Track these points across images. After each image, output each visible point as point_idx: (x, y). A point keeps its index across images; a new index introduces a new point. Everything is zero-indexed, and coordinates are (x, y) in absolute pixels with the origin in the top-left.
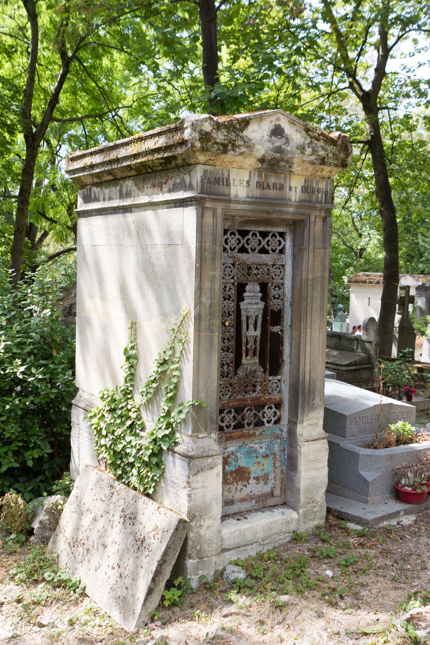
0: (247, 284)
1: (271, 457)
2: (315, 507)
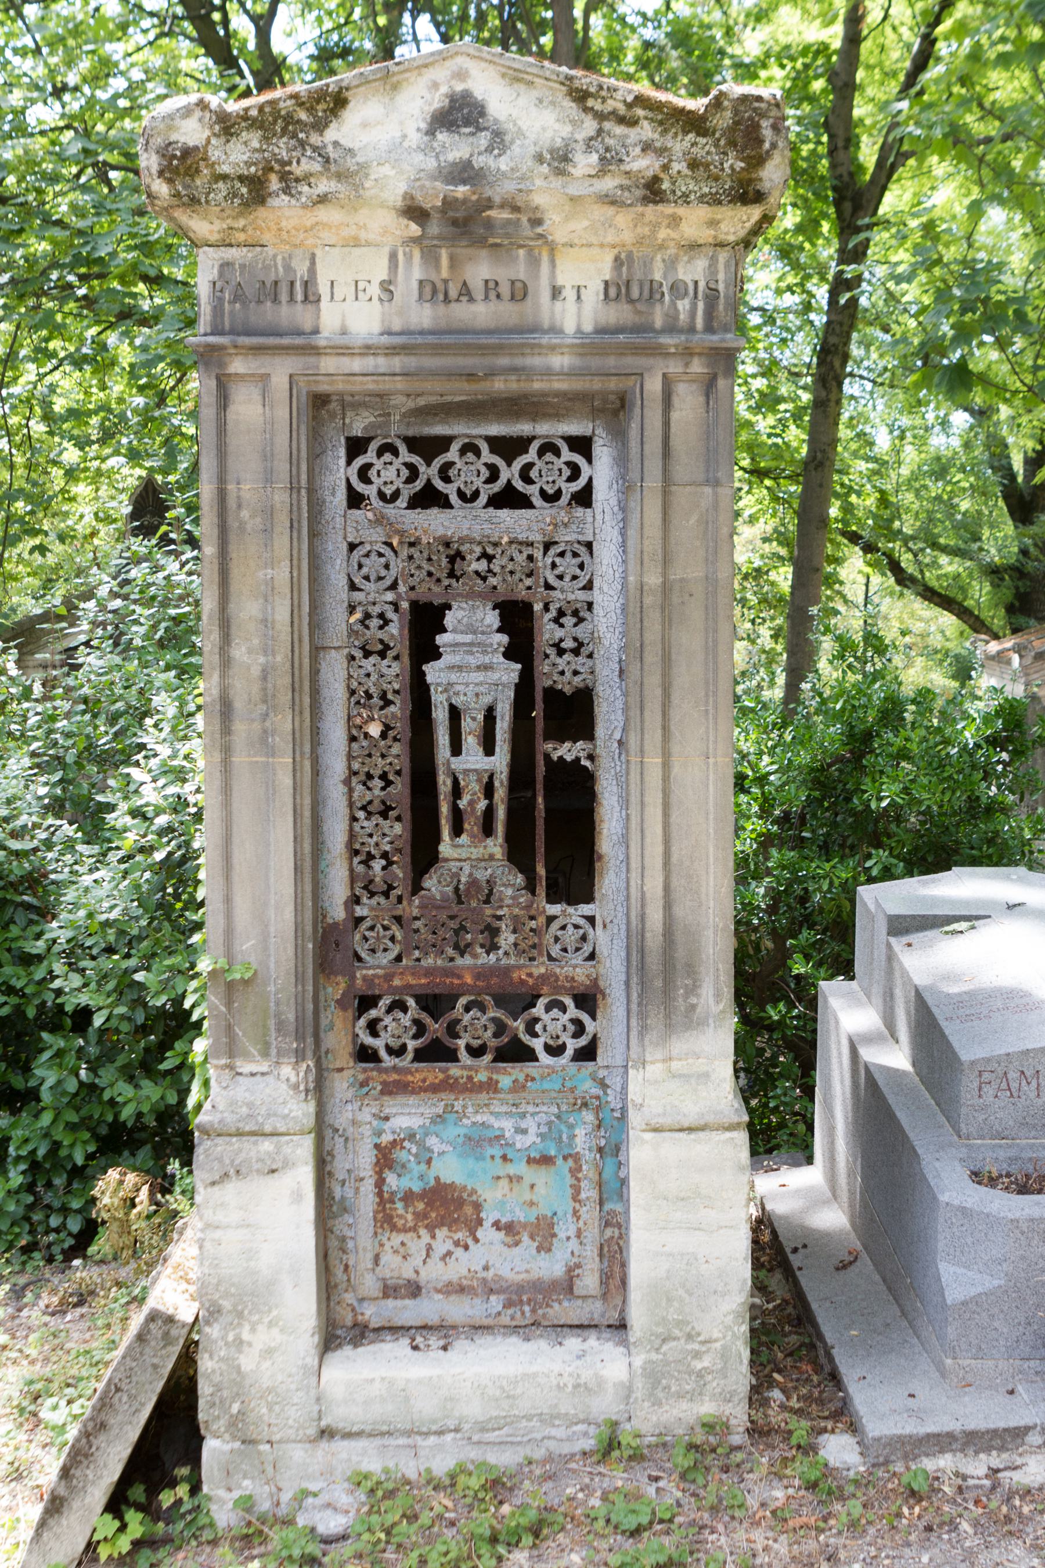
1: (563, 1167)
2: (697, 1355)
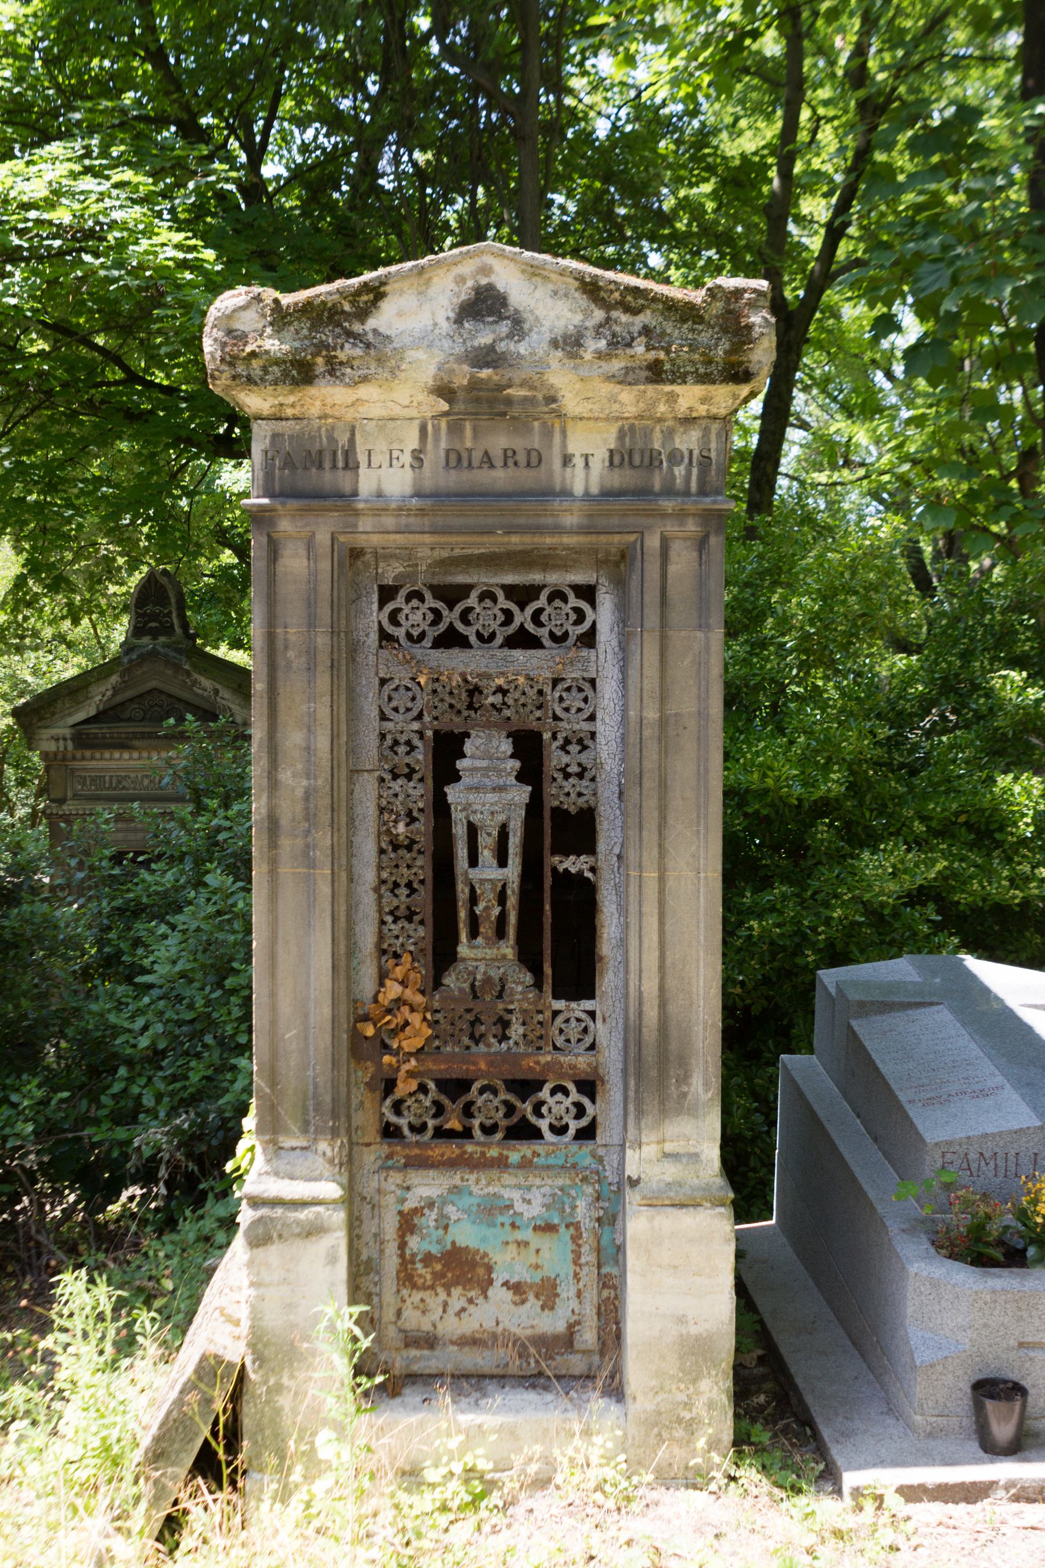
0: (468, 735)
1: (565, 1234)
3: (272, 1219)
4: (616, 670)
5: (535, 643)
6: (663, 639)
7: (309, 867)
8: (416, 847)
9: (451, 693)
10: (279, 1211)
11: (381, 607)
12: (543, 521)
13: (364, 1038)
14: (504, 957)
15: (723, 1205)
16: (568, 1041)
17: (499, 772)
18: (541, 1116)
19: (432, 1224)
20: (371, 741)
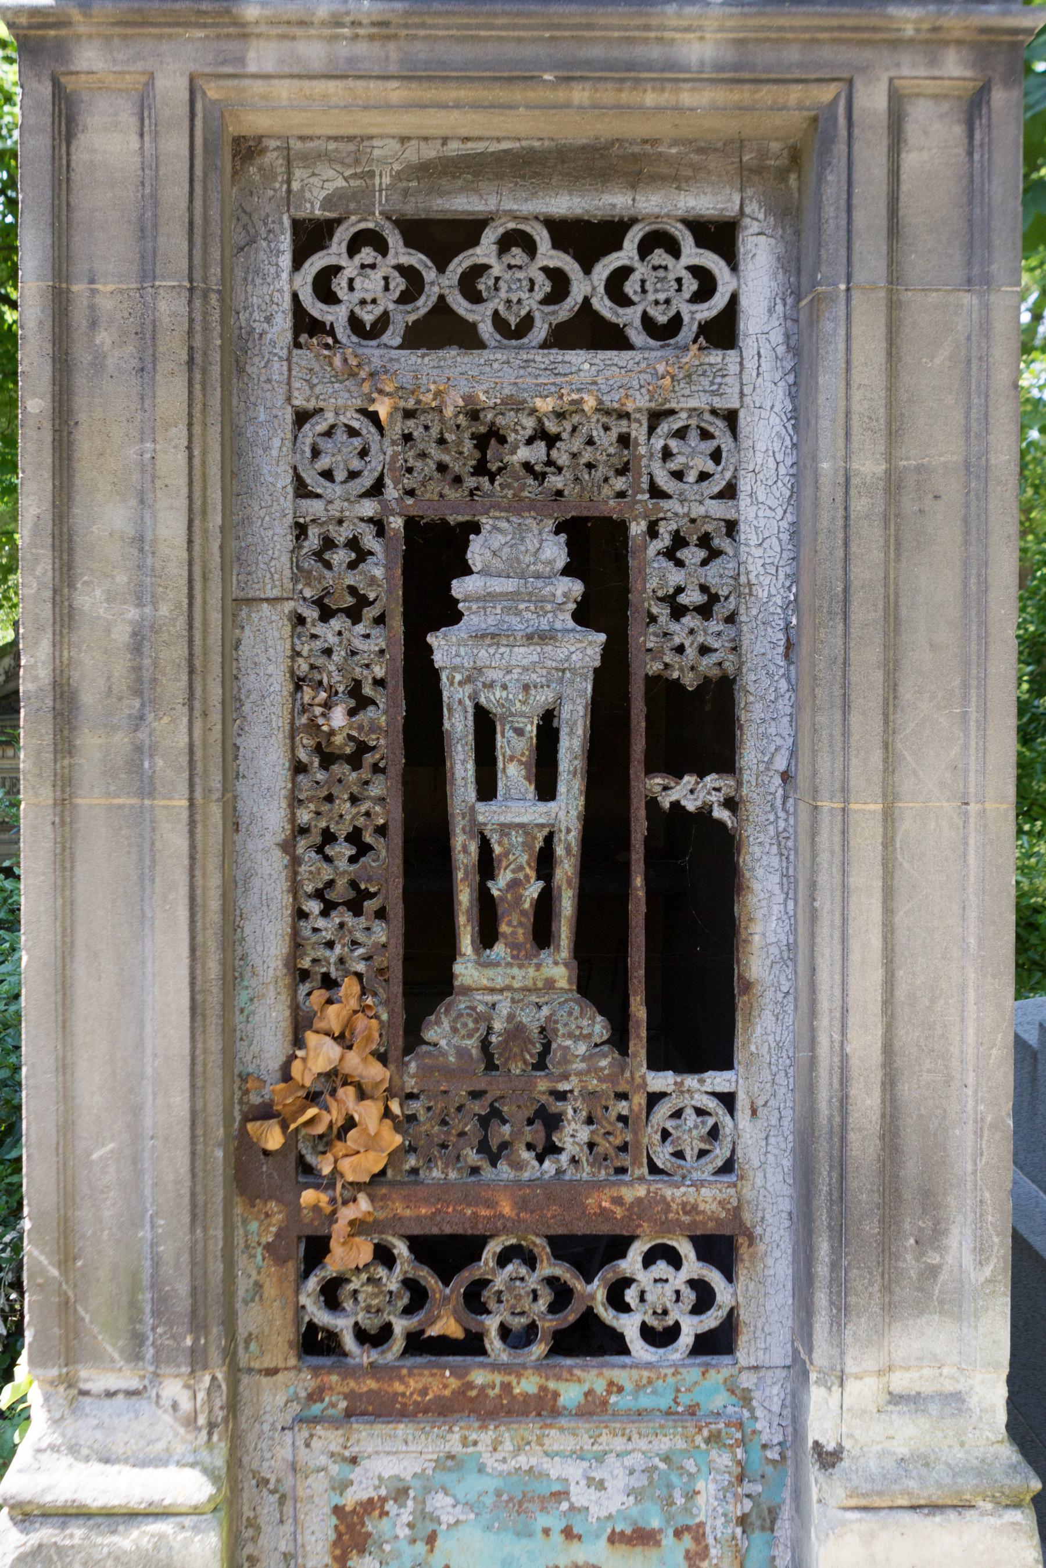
0: (475, 528)
3: (60, 1550)
4: (780, 392)
5: (612, 338)
6: (893, 305)
7: (141, 794)
8: (369, 759)
9: (441, 441)
10: (77, 1534)
11: (298, 263)
12: (640, 52)
13: (260, 1154)
14: (550, 984)
15: (1017, 1506)
16: (679, 1155)
17: (539, 602)
18: (623, 1308)
19: (403, 1532)
20: (277, 539)
